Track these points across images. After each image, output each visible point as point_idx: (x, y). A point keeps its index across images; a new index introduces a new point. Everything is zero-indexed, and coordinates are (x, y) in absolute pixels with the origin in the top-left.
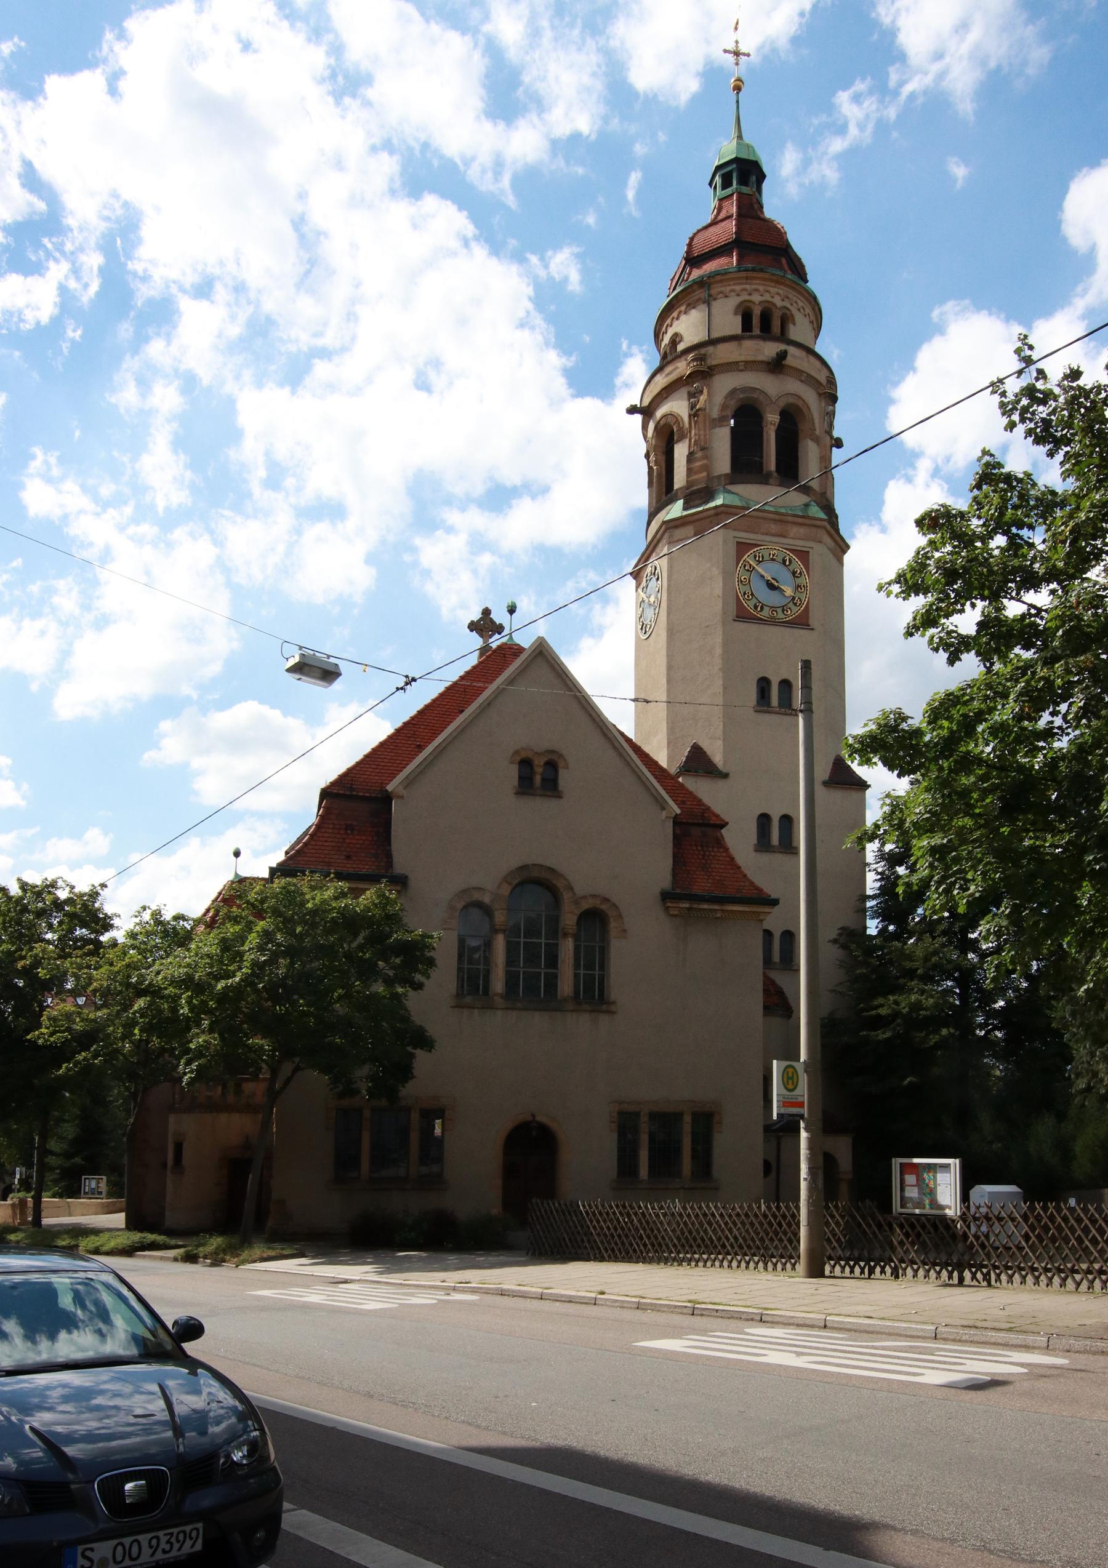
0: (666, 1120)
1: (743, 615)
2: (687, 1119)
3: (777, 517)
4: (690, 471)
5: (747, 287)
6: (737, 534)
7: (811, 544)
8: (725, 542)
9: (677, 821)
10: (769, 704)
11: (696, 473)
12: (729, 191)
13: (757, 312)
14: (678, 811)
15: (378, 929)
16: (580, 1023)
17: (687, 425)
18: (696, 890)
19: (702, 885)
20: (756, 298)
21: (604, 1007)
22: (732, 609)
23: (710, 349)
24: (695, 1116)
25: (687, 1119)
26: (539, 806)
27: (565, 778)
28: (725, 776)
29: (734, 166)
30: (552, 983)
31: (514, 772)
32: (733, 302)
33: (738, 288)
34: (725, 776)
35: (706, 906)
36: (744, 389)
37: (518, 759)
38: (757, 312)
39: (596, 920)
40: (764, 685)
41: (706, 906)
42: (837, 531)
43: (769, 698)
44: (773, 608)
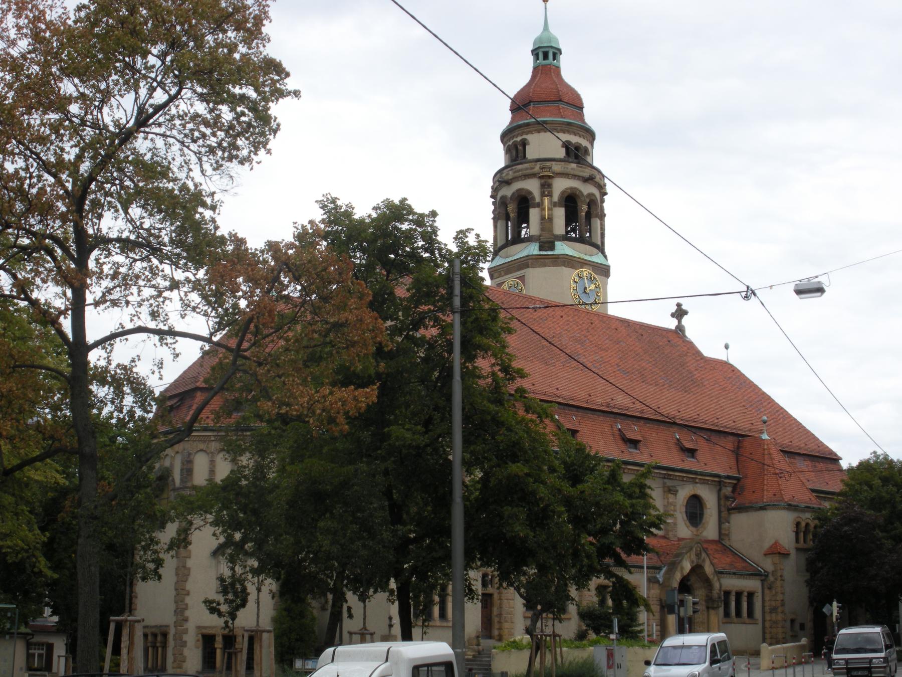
36: (571, 188)
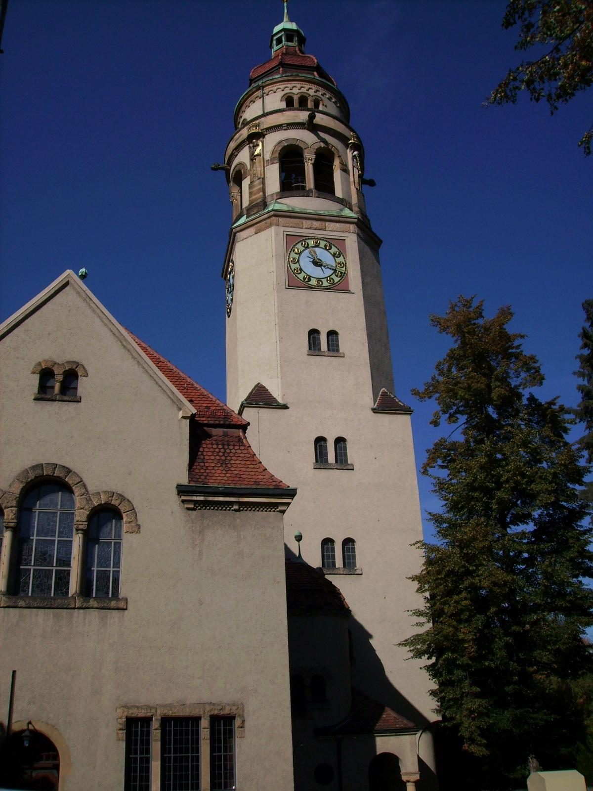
0: (180, 729)
1: (293, 284)
2: (205, 723)
3: (317, 217)
4: (251, 194)
5: (289, 85)
6: (286, 229)
7: (346, 234)
8: (277, 234)
9: (192, 419)
10: (320, 349)
11: (255, 194)
12: (280, 46)
13: (296, 98)
14: (194, 411)
15: (589, 717)
16: (87, 623)
17: (249, 168)
18: (212, 484)
19: (218, 478)
20: (295, 91)
21: (113, 604)
22: (284, 278)
23: (263, 119)
24: (215, 720)
25: (205, 723)
26: (57, 411)
27: (83, 386)
28: (285, 407)
29: (283, 33)
30: (63, 579)
31: (35, 380)
32: (280, 94)
33: (282, 87)
34: (285, 407)
35: (221, 499)
37: (39, 369)
38: (296, 98)
39: (107, 515)
40: (313, 334)
41: (221, 499)
42: (370, 229)
43: (319, 344)
44: (319, 280)
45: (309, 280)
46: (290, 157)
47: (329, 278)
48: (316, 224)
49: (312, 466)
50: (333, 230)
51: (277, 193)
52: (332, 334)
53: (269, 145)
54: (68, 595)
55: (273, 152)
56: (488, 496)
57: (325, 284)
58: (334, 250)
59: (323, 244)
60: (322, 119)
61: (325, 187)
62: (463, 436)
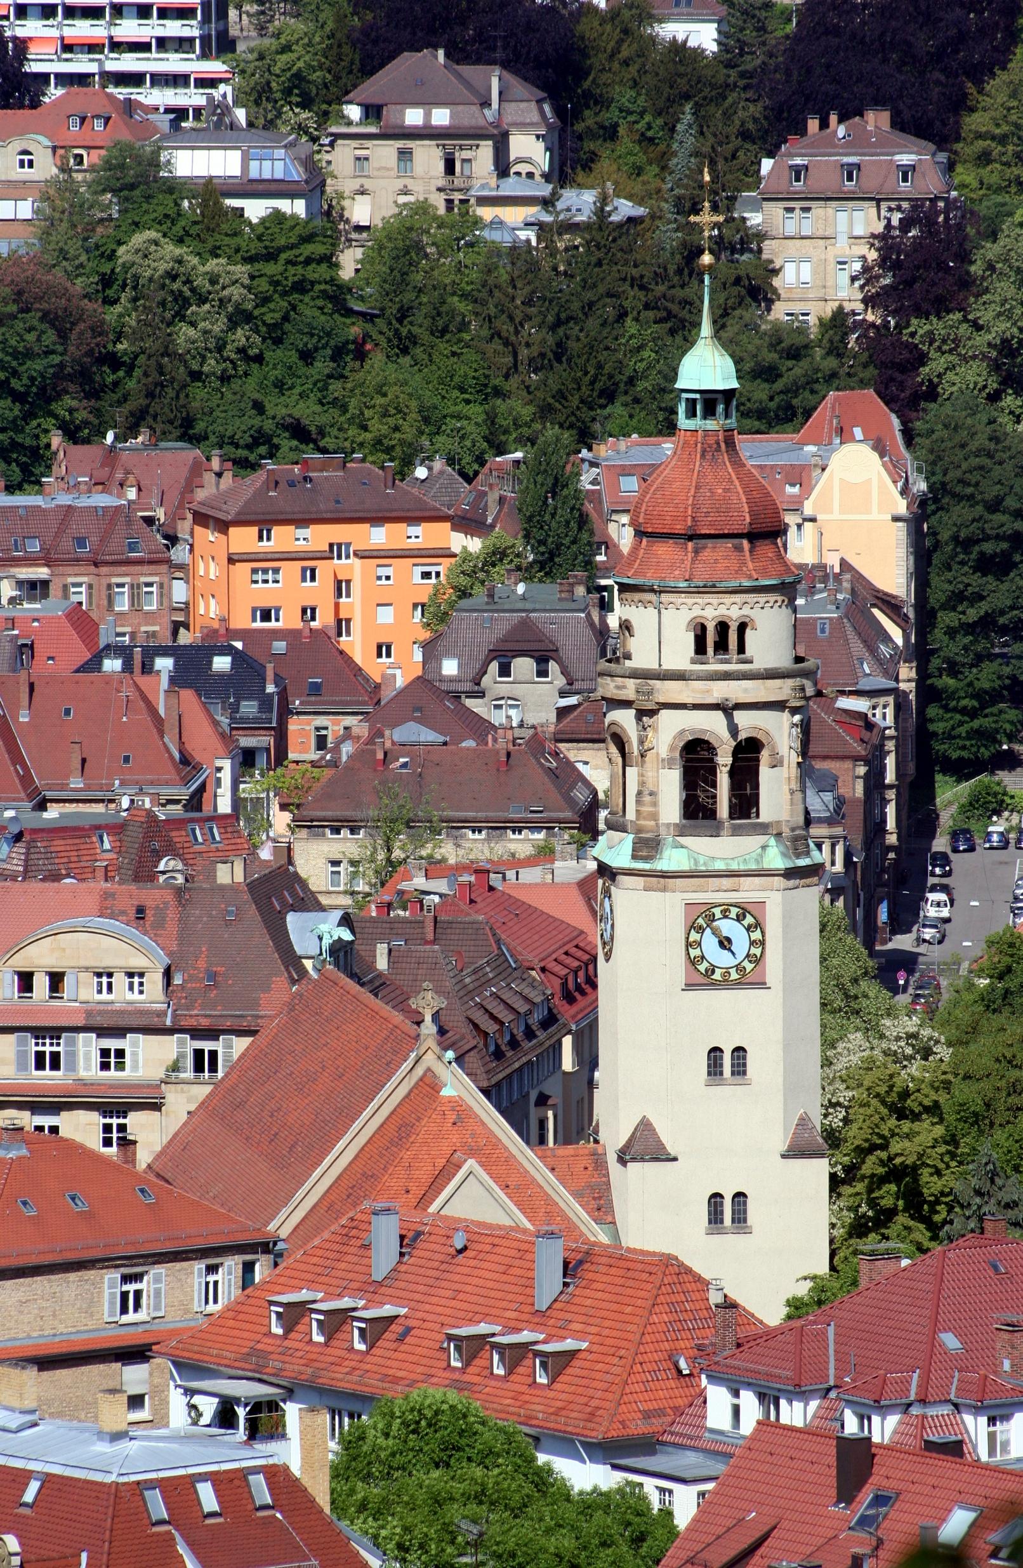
5: (699, 601)
34: (675, 1159)
45: (713, 972)
46: (696, 757)
47: (739, 968)
48: (726, 882)
49: (703, 1231)
50: (749, 891)
51: (676, 825)
52: (739, 1051)
53: (670, 729)
54: (734, 390)
55: (672, 748)
56: (892, 855)
57: (734, 975)
58: (749, 920)
59: (734, 911)
60: (746, 690)
61: (745, 803)
62: (848, 448)
